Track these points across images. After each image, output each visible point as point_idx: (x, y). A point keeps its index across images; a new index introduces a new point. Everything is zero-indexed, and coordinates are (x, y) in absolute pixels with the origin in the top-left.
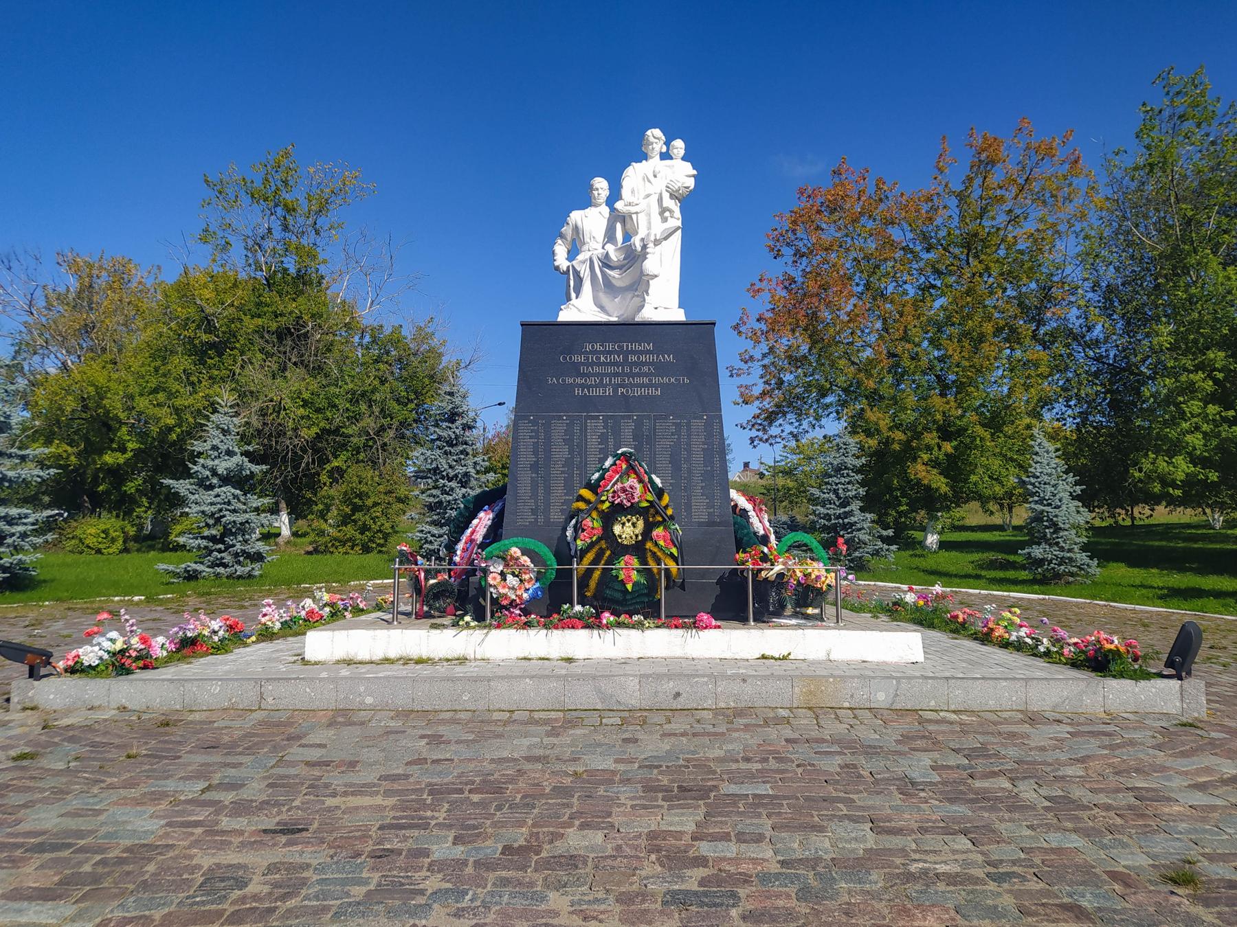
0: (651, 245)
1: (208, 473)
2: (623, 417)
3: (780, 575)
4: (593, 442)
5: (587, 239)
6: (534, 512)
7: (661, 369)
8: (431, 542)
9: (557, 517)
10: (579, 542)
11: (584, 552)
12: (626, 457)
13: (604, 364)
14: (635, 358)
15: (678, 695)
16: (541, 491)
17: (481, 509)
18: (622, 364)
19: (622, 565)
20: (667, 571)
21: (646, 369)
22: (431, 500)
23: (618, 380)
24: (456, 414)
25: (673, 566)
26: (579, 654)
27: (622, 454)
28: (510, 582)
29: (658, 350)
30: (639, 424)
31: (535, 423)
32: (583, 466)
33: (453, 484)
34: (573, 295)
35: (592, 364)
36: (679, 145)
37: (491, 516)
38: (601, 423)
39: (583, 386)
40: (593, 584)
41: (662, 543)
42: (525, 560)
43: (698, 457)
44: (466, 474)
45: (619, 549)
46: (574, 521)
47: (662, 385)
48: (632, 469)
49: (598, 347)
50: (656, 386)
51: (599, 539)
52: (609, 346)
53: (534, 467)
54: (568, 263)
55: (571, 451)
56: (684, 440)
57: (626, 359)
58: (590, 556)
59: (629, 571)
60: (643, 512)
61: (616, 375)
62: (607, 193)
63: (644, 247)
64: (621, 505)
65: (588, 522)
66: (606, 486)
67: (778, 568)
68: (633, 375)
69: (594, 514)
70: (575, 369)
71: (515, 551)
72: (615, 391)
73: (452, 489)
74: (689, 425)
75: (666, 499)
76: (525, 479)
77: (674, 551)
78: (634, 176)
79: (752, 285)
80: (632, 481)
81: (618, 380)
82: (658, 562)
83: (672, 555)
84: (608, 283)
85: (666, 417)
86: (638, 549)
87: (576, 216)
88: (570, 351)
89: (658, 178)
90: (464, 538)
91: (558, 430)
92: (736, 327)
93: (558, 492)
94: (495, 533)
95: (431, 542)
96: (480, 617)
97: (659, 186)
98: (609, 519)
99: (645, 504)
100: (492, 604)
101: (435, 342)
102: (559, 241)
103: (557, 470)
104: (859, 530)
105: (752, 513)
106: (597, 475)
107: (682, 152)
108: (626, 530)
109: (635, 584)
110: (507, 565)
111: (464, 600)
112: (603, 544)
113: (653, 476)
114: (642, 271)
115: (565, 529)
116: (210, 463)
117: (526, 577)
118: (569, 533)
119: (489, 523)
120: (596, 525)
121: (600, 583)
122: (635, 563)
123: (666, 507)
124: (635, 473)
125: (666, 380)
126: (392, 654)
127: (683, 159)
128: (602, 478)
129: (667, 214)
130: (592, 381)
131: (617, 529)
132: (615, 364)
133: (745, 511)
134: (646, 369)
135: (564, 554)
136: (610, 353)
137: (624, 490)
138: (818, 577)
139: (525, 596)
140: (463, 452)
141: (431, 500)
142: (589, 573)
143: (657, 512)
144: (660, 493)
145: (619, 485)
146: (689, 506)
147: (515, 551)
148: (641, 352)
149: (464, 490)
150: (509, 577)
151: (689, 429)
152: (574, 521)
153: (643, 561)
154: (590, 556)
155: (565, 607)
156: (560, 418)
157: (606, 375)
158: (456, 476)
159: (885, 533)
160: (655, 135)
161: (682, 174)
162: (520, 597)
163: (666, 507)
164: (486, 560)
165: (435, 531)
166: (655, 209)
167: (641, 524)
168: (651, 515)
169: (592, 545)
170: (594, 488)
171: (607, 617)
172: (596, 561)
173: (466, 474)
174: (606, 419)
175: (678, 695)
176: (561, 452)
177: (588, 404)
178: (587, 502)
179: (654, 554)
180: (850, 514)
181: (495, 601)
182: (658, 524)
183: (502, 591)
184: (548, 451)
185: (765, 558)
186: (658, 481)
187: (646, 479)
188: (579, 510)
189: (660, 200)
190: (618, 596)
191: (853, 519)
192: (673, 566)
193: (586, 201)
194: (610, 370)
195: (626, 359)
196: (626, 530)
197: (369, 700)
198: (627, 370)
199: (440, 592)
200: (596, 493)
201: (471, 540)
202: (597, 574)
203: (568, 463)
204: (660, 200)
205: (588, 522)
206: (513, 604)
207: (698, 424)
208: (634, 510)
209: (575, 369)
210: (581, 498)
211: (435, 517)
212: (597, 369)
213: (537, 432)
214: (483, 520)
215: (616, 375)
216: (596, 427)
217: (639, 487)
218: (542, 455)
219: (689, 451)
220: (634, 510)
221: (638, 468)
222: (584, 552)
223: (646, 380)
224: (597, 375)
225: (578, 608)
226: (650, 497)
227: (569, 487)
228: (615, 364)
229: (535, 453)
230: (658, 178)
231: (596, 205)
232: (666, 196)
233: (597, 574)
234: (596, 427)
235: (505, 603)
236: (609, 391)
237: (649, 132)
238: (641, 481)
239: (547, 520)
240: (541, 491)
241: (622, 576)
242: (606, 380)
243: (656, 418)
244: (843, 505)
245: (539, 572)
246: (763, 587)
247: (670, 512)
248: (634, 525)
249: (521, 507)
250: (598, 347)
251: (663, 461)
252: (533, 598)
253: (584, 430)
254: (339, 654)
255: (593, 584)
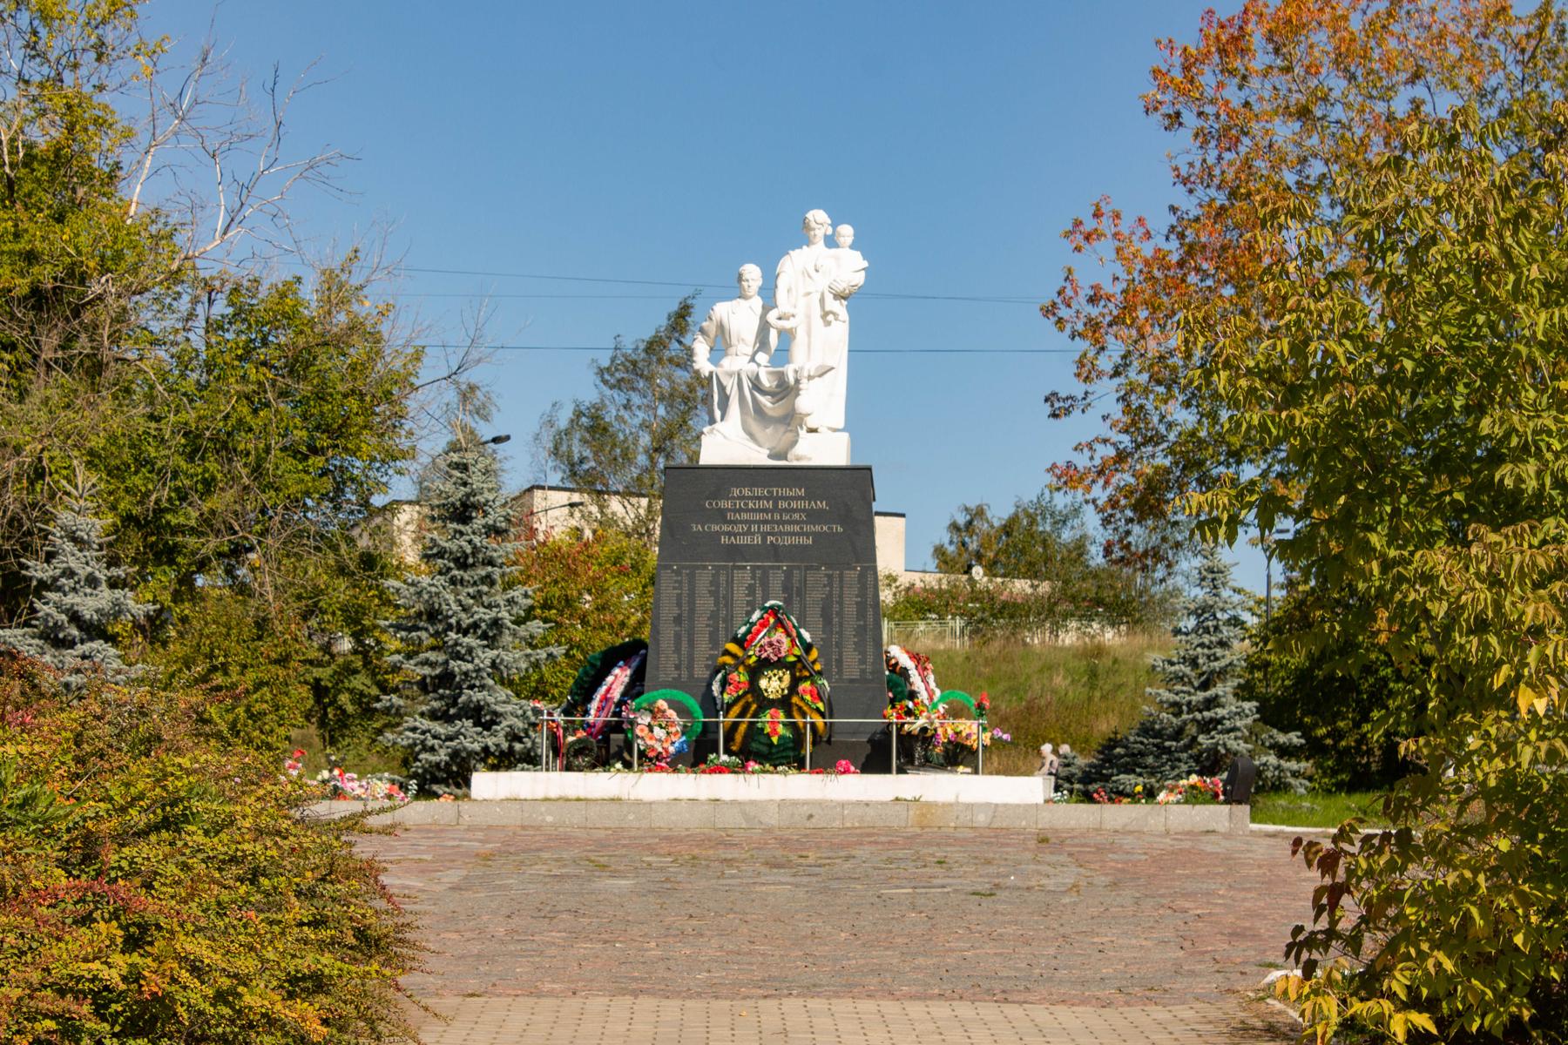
0: (804, 381)
1: (64, 617)
2: (772, 567)
3: (924, 730)
4: (740, 594)
5: (734, 341)
6: (678, 667)
7: (813, 516)
8: (432, 749)
9: (701, 672)
10: (726, 696)
11: (730, 706)
12: (774, 611)
13: (752, 510)
14: (785, 505)
15: (811, 816)
16: (684, 645)
17: (614, 665)
18: (772, 511)
19: (768, 718)
20: (813, 725)
21: (796, 516)
22: (427, 671)
23: (767, 528)
24: (475, 507)
25: (819, 721)
26: (727, 796)
27: (771, 607)
28: (658, 730)
29: (809, 497)
30: (789, 575)
31: (678, 573)
32: (729, 619)
33: (469, 640)
34: (718, 414)
35: (740, 510)
36: (846, 232)
37: (629, 672)
38: (748, 574)
39: (729, 534)
40: (739, 737)
41: (808, 697)
42: (672, 714)
43: (851, 609)
44: (496, 623)
45: (765, 704)
46: (719, 676)
47: (814, 534)
48: (780, 623)
49: (746, 492)
50: (807, 535)
51: (745, 694)
52: (758, 491)
53: (678, 620)
54: (712, 368)
55: (717, 603)
56: (836, 592)
57: (775, 504)
58: (736, 709)
59: (775, 724)
60: (791, 667)
61: (765, 522)
62: (760, 283)
63: (797, 381)
64: (767, 659)
65: (734, 676)
66: (753, 639)
67: (922, 721)
68: (784, 523)
69: (741, 669)
70: (721, 516)
71: (662, 704)
72: (764, 539)
73: (470, 650)
74: (841, 577)
75: (814, 654)
76: (668, 632)
77: (821, 705)
78: (793, 265)
79: (1078, 223)
80: (779, 635)
81: (767, 528)
82: (804, 715)
83: (818, 710)
84: (759, 410)
85: (818, 569)
86: (784, 703)
87: (722, 310)
88: (717, 495)
89: (823, 269)
90: (598, 697)
91: (703, 580)
92: (1049, 311)
93: (703, 647)
94: (635, 688)
95: (432, 749)
96: (628, 765)
97: (821, 283)
98: (755, 672)
99: (792, 659)
100: (640, 758)
101: (365, 308)
102: (700, 338)
103: (702, 624)
104: (1229, 731)
105: (914, 674)
106: (743, 629)
107: (849, 240)
108: (773, 684)
109: (781, 737)
110: (654, 718)
111: (608, 748)
112: (749, 698)
113: (802, 631)
114: (794, 409)
115: (710, 685)
116: (70, 599)
117: (673, 730)
118: (716, 687)
119: (627, 680)
120: (743, 679)
121: (746, 736)
122: (782, 717)
123: (814, 662)
124: (783, 627)
125: (818, 528)
126: (553, 795)
127: (852, 247)
128: (749, 632)
129: (830, 317)
130: (739, 528)
131: (763, 683)
132: (765, 511)
133: (906, 669)
134: (796, 516)
135: (710, 705)
136: (759, 498)
137: (771, 644)
138: (969, 736)
139: (672, 749)
140: (489, 580)
141: (427, 671)
142: (735, 725)
143: (804, 667)
144: (808, 648)
145: (766, 640)
146: (840, 662)
147: (662, 704)
148: (792, 498)
149: (492, 654)
150: (657, 730)
151: (841, 581)
152: (719, 676)
153: (789, 714)
154: (736, 709)
155: (712, 756)
156: (705, 567)
157: (755, 522)
158: (475, 626)
159: (1282, 738)
160: (818, 217)
161: (849, 267)
162: (666, 750)
163: (814, 662)
164: (634, 711)
165: (440, 728)
166: (817, 312)
167: (787, 678)
168: (798, 670)
169: (739, 698)
170: (741, 642)
171: (753, 766)
172: (742, 714)
173: (496, 623)
174: (754, 568)
175: (811, 816)
176: (705, 604)
177: (735, 552)
178: (734, 656)
179: (800, 708)
180: (1211, 703)
181: (642, 754)
182: (806, 679)
183: (650, 742)
184: (692, 603)
185: (909, 713)
186: (807, 636)
187: (794, 634)
188: (724, 666)
189: (822, 301)
190: (764, 749)
191: (1221, 712)
192: (819, 721)
193: (736, 289)
194: (758, 517)
195: (775, 504)
196: (773, 684)
197: (549, 819)
198: (777, 517)
199: (580, 749)
200: (744, 649)
201: (605, 699)
202: (742, 728)
203: (714, 616)
204: (822, 301)
205: (734, 676)
206: (659, 757)
207: (851, 575)
208: (781, 664)
209: (721, 516)
210: (727, 653)
211: (436, 704)
212: (745, 516)
213: (680, 582)
214: (619, 678)
215: (765, 522)
216: (743, 578)
217: (786, 642)
218: (685, 607)
219: (841, 603)
220: (781, 664)
221: (786, 622)
222: (730, 706)
223: (797, 528)
224: (746, 522)
225: (724, 758)
226: (797, 651)
227: (714, 642)
228: (765, 511)
229: (679, 605)
230: (823, 269)
231: (743, 296)
232: (829, 298)
233: (742, 728)
234: (743, 578)
235: (652, 755)
236: (758, 540)
237: (810, 215)
238: (789, 635)
239: (691, 676)
240: (684, 645)
241: (768, 730)
242: (754, 528)
243: (807, 568)
244: (1205, 686)
245: (685, 726)
246: (907, 740)
247: (818, 667)
248: (780, 679)
249: (663, 661)
250: (746, 492)
251: (814, 614)
252: (679, 752)
253: (730, 583)
254: (502, 794)
255: (739, 737)
